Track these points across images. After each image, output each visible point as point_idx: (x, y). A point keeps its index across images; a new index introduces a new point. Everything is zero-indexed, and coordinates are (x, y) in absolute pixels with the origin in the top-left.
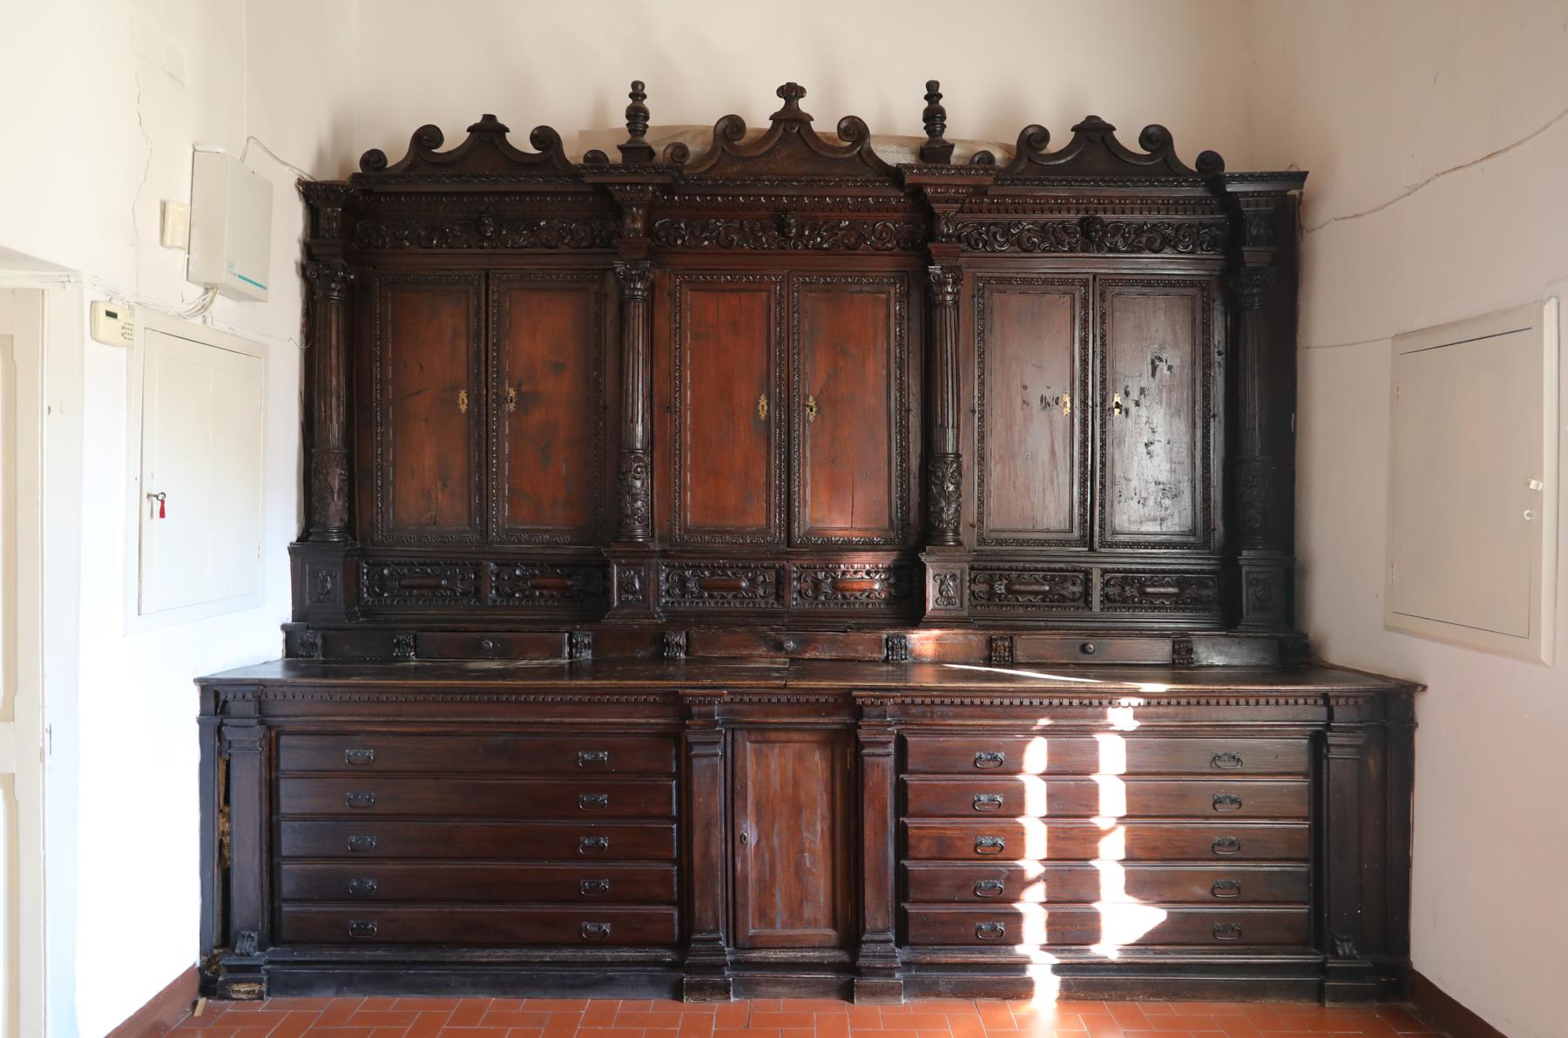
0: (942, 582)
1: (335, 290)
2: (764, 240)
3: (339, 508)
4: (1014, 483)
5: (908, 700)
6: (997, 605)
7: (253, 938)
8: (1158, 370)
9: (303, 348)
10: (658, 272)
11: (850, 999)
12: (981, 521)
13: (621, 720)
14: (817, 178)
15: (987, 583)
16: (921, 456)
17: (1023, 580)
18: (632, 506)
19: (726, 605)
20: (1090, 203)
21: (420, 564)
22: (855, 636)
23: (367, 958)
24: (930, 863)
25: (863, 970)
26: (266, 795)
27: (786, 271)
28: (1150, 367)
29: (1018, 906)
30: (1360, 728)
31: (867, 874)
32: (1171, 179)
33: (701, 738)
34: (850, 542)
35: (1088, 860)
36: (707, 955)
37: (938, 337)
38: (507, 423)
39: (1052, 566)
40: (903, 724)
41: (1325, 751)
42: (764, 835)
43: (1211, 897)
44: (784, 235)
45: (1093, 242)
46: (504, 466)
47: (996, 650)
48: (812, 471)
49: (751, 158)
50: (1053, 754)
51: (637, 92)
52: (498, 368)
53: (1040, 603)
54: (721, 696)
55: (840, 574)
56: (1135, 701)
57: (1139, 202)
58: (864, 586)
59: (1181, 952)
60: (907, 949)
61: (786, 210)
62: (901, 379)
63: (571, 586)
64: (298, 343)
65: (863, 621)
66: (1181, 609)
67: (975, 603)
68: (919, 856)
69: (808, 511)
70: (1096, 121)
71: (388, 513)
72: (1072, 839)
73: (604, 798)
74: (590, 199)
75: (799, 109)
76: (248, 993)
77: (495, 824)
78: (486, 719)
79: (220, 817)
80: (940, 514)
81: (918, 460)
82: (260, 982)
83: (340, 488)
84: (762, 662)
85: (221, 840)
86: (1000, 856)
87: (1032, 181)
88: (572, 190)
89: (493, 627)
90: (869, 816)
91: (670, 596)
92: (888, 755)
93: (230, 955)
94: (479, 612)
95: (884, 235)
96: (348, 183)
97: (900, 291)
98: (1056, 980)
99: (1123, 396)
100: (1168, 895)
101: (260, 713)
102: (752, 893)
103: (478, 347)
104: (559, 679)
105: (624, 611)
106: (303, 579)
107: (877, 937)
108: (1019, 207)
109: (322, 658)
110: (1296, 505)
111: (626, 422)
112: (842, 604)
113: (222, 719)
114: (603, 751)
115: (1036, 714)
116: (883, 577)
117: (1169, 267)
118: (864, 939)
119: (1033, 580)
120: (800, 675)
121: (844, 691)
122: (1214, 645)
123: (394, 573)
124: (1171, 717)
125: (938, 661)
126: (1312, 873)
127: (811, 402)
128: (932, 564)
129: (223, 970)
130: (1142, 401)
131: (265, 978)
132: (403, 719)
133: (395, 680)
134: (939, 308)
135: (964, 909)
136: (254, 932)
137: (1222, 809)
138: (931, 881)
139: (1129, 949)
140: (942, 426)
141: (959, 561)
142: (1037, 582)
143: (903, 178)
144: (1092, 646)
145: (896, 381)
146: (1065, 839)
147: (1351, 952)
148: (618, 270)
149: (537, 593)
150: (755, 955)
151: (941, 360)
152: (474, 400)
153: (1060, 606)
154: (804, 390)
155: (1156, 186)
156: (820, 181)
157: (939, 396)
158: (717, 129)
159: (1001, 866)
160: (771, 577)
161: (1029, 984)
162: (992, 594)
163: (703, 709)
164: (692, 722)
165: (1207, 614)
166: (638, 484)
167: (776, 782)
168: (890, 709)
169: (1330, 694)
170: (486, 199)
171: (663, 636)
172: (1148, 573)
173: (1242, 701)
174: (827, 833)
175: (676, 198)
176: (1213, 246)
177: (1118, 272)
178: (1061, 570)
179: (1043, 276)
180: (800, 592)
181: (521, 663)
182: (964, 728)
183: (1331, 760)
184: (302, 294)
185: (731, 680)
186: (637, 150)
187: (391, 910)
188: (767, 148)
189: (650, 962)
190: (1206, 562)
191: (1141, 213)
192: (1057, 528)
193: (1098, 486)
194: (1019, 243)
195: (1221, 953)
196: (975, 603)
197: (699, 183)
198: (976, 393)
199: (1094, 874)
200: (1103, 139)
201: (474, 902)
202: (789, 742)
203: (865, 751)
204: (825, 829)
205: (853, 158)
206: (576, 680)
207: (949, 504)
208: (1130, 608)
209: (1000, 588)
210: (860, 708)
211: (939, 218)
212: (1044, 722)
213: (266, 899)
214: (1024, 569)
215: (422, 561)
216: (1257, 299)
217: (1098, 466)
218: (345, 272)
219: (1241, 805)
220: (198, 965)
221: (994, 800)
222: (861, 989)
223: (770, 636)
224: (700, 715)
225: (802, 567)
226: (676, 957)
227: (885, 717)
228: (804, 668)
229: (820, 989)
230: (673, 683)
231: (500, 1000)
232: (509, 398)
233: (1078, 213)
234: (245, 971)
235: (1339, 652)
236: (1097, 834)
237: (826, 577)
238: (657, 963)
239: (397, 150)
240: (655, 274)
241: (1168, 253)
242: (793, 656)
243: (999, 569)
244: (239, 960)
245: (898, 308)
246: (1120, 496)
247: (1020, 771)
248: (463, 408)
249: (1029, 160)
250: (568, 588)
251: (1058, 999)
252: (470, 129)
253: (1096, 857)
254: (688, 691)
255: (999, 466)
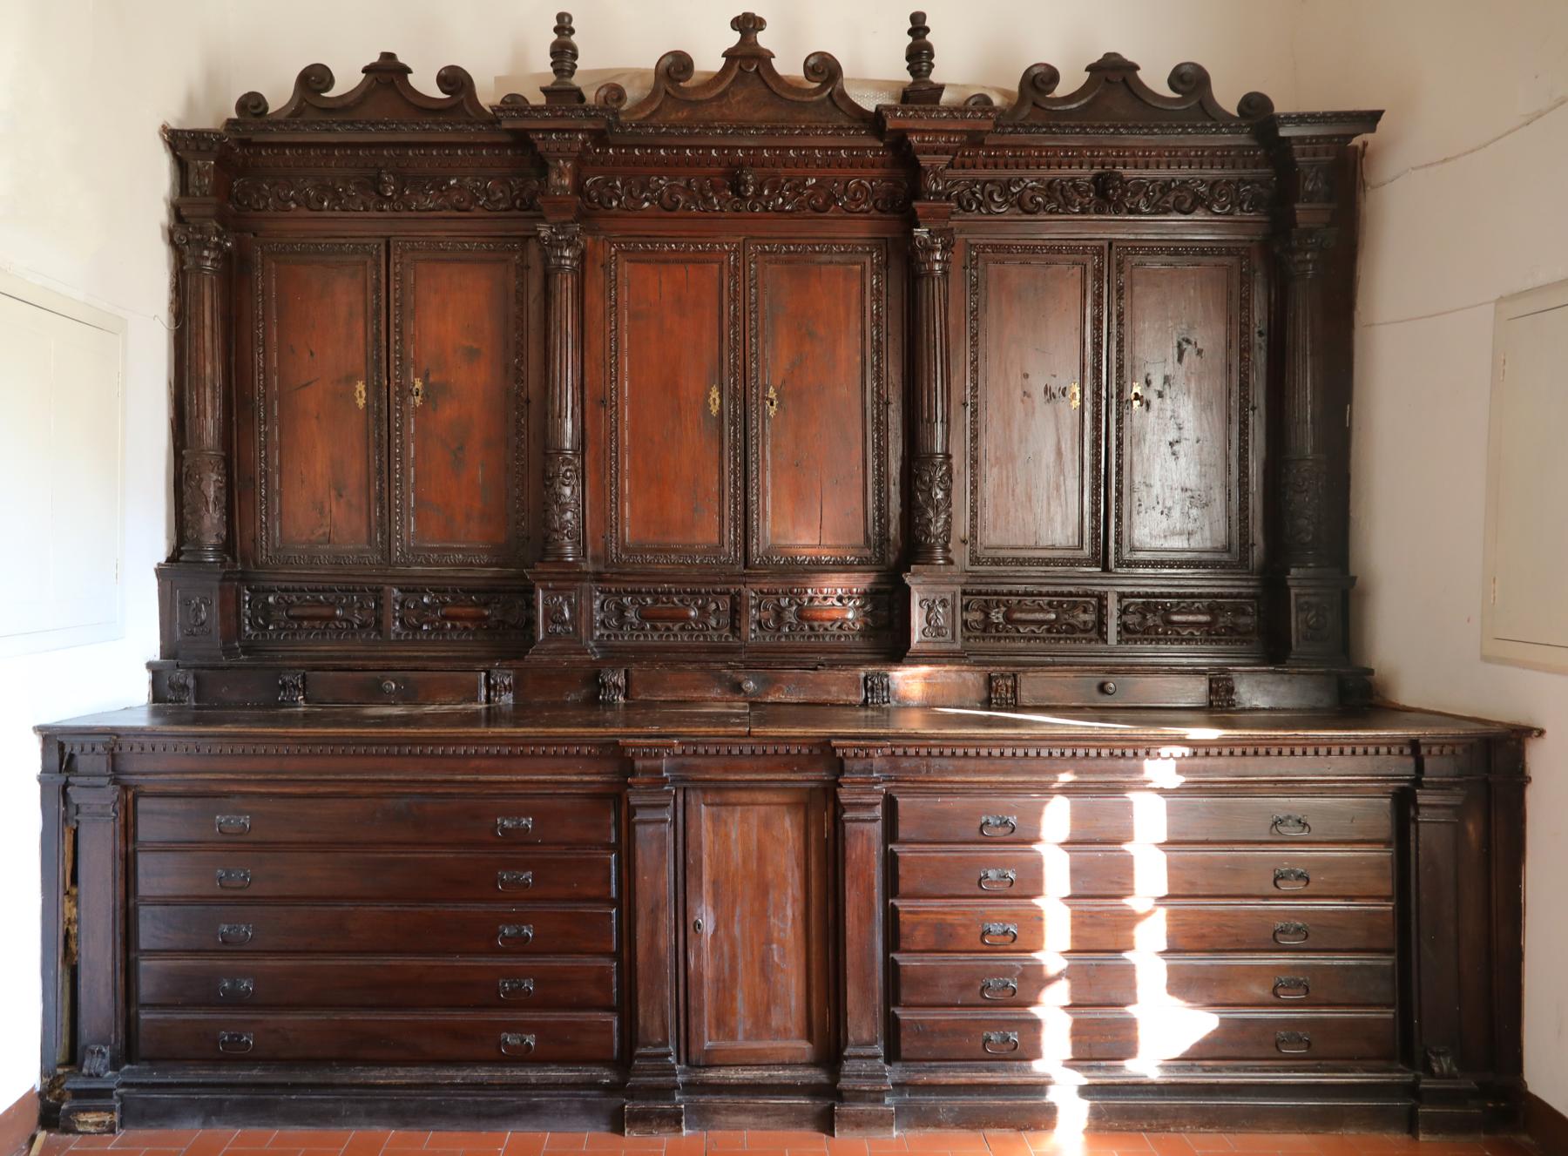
0: (930, 609)
1: (207, 258)
2: (715, 201)
3: (216, 521)
4: (1013, 491)
5: (899, 751)
6: (994, 637)
7: (104, 1055)
8: (1186, 354)
9: (173, 328)
10: (589, 239)
11: (829, 1130)
12: (973, 536)
13: (549, 777)
14: (780, 125)
15: (982, 611)
16: (903, 458)
17: (1024, 607)
18: (560, 518)
19: (672, 639)
20: (1107, 155)
21: (311, 591)
22: (825, 675)
23: (240, 1080)
24: (926, 957)
25: (845, 1094)
26: (121, 873)
27: (742, 238)
28: (1176, 350)
29: (1034, 1010)
30: (1455, 784)
31: (850, 971)
32: (1209, 125)
33: (646, 800)
34: (818, 562)
35: (1120, 951)
36: (653, 1076)
37: (924, 313)
38: (412, 420)
39: (1059, 589)
40: (893, 781)
41: (1412, 813)
42: (722, 922)
43: (1273, 999)
44: (739, 194)
45: (1108, 200)
46: (410, 472)
47: (997, 690)
48: (773, 477)
49: (700, 102)
50: (1076, 817)
51: (564, 26)
52: (401, 353)
53: (1045, 635)
54: (671, 746)
55: (806, 600)
56: (1178, 751)
57: (1167, 154)
58: (835, 615)
59: (1236, 1069)
60: (898, 1066)
61: (741, 165)
62: (878, 365)
63: (488, 617)
64: (166, 322)
65: (835, 657)
66: (1215, 641)
67: (967, 634)
68: (913, 948)
69: (769, 524)
70: (1114, 59)
71: (274, 529)
72: (1102, 925)
73: (528, 876)
74: (509, 152)
75: (757, 43)
76: (97, 1124)
77: (396, 908)
78: (385, 777)
79: (66, 900)
80: (927, 526)
81: (899, 463)
82: (111, 1110)
83: (216, 498)
84: (717, 707)
85: (67, 929)
86: (1013, 947)
87: (1039, 127)
88: (486, 140)
89: (395, 664)
90: (852, 897)
91: (605, 627)
92: (874, 820)
93: (77, 1075)
94: (380, 648)
95: (858, 195)
96: (222, 131)
97: (878, 261)
98: (1084, 1106)
99: (1144, 385)
100: (1219, 997)
101: (113, 770)
102: (708, 994)
103: (378, 329)
104: (473, 726)
105: (552, 646)
106: (173, 607)
107: (862, 1052)
108: (1022, 161)
109: (194, 704)
110: (1351, 514)
111: (553, 417)
112: (809, 637)
113: (67, 778)
114: (526, 816)
115: (1055, 768)
116: (858, 603)
117: (1201, 231)
118: (846, 1054)
119: (1037, 607)
120: (762, 721)
121: (822, 740)
122: (1259, 683)
123: (281, 601)
124: (1223, 770)
125: (927, 706)
126: (1396, 968)
127: (772, 394)
128: (917, 587)
129: (68, 1096)
130: (1167, 391)
131: (118, 1105)
132: (285, 777)
133: (274, 727)
134: (925, 279)
135: (969, 1014)
136: (105, 1045)
137: (1285, 887)
138: (927, 980)
139: (1168, 1066)
140: (929, 420)
141: (952, 583)
142: (1041, 609)
143: (884, 122)
144: (1112, 685)
145: (872, 367)
146: (1093, 925)
147: (1450, 1069)
148: (542, 235)
149: (449, 625)
150: (712, 1075)
151: (928, 340)
152: (374, 391)
153: (1069, 639)
154: (764, 379)
155: (1189, 133)
156: (783, 128)
157: (926, 383)
158: (660, 66)
159: (1014, 960)
160: (724, 605)
161: (1051, 1110)
162: (987, 625)
163: (648, 763)
164: (635, 780)
165: (1245, 646)
166: (567, 491)
167: (737, 854)
168: (878, 762)
169: (1421, 741)
170: (385, 153)
171: (597, 675)
172: (1174, 598)
173: (1310, 750)
174: (799, 918)
175: (611, 151)
176: (1255, 206)
177: (1139, 237)
178: (1070, 594)
179: (1047, 243)
180: (759, 623)
181: (429, 709)
182: (966, 786)
183: (1421, 825)
184: (169, 264)
185: (684, 726)
186: (562, 94)
187: (270, 1018)
188: (720, 90)
189: (583, 1084)
190: (1245, 583)
191: (1169, 167)
192: (1064, 544)
193: (1113, 493)
194: (1020, 204)
195: (1287, 1070)
196: (967, 634)
197: (638, 131)
198: (968, 383)
199: (1129, 970)
200: (1124, 80)
201: (371, 1007)
202: (753, 804)
203: (847, 816)
204: (796, 914)
205: (823, 101)
206: (494, 727)
207: (937, 514)
208: (1152, 640)
209: (997, 616)
210: (841, 760)
211: (926, 173)
212: (1066, 777)
213: (120, 1004)
214: (1026, 594)
215: (313, 586)
216: (1311, 266)
217: (1114, 470)
218: (220, 236)
219: (1308, 881)
220: (38, 1088)
221: (1005, 877)
222: (844, 1119)
223: (725, 675)
224: (645, 771)
225: (762, 592)
226: (615, 1078)
227: (871, 772)
228: (763, 711)
229: (792, 1119)
230: (612, 730)
231: (401, 1132)
232: (414, 390)
233: (1092, 168)
234: (93, 1097)
235: (1409, 693)
236: (1132, 919)
237: (790, 605)
238: (592, 1085)
239: (279, 93)
240: (585, 241)
241: (1199, 215)
242: (753, 699)
243: (996, 593)
244: (86, 1083)
245: (874, 282)
246: (1140, 505)
247: (1037, 840)
248: (361, 402)
249: (1035, 104)
250: (486, 618)
251: (1086, 1129)
252: (366, 70)
253: (1131, 948)
254: (631, 741)
255: (995, 470)
